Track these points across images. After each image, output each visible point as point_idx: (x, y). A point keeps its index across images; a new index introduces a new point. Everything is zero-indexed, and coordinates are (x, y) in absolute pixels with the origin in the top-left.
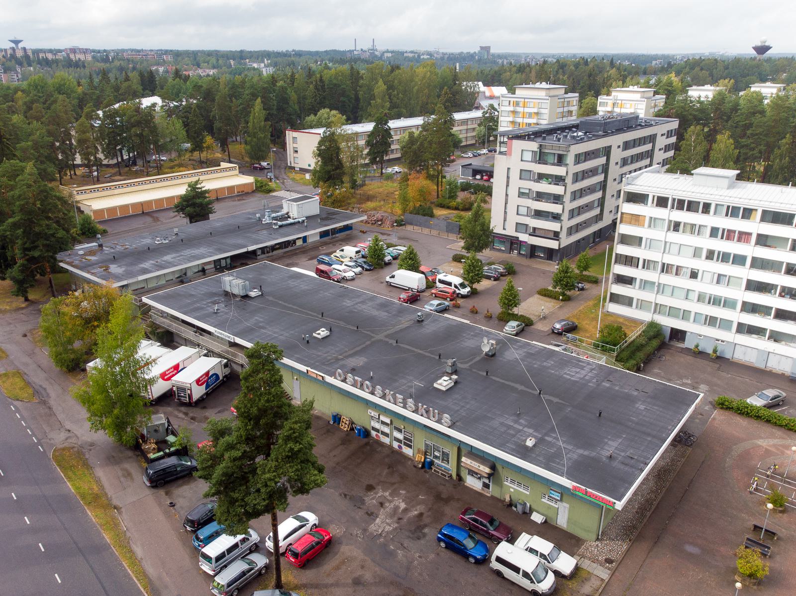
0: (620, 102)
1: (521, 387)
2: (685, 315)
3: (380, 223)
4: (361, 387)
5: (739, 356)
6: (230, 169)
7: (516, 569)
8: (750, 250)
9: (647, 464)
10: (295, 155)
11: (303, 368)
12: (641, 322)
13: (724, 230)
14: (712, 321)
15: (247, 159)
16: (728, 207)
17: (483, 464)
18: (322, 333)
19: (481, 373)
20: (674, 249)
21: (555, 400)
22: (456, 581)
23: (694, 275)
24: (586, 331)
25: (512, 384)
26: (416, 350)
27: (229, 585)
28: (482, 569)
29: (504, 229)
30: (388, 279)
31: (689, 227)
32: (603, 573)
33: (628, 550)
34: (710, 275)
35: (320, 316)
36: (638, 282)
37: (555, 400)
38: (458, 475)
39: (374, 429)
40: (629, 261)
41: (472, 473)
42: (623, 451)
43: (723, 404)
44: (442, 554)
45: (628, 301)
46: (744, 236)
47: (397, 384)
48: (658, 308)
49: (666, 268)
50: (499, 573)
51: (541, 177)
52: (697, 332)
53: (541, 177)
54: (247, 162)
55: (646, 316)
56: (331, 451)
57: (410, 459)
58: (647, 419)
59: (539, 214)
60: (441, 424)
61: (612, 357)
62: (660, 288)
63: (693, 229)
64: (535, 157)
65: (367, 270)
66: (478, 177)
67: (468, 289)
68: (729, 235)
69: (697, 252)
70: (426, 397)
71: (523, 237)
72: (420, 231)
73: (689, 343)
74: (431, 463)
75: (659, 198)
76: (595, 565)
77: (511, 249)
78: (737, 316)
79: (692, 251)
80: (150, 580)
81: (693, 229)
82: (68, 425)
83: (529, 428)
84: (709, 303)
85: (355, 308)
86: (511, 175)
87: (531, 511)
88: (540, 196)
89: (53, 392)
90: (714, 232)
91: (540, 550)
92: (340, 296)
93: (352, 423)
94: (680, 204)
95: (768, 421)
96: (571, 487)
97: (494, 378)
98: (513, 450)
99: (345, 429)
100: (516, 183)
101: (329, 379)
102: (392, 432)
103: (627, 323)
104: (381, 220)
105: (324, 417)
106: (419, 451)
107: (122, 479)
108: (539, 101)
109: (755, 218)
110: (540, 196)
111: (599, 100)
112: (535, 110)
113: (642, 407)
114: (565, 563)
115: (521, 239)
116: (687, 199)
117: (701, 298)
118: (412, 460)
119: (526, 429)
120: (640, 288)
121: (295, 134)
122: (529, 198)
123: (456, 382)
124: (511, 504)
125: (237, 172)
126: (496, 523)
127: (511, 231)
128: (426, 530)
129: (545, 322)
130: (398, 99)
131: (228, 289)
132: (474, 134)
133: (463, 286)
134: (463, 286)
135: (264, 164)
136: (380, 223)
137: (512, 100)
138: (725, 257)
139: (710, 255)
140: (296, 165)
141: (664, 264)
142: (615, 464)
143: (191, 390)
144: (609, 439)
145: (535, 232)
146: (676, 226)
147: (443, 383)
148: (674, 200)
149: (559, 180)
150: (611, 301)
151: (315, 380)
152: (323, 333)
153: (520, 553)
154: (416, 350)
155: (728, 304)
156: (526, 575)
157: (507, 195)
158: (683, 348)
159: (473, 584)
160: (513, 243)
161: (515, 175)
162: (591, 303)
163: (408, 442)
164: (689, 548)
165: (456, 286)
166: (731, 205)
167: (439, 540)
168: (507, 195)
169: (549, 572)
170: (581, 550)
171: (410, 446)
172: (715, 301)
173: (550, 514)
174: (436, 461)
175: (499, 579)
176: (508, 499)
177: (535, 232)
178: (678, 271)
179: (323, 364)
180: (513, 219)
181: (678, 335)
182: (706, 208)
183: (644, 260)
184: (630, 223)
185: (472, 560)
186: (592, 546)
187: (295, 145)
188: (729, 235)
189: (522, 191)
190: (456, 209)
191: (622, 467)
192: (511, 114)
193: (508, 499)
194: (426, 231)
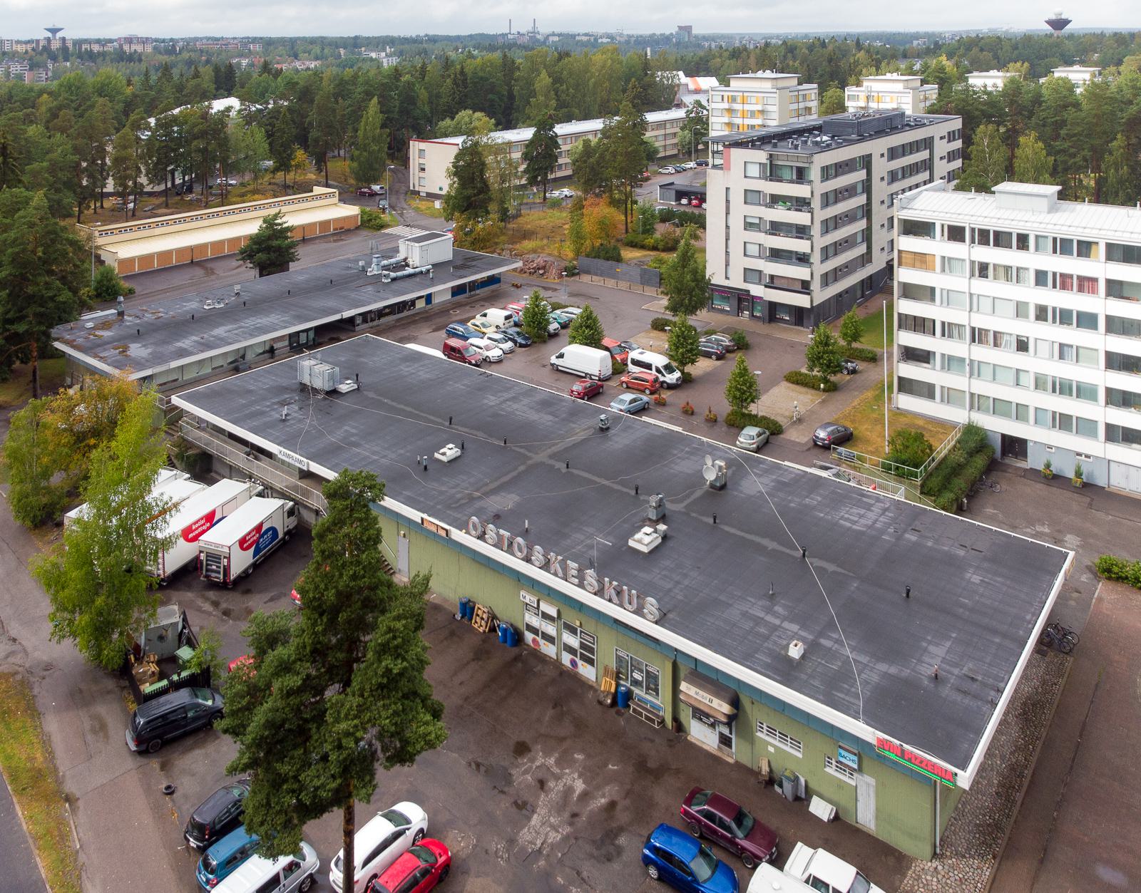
1: (771, 545)
2: (1020, 412)
3: (541, 272)
4: (510, 550)
6: (326, 196)
10: (422, 174)
11: (415, 515)
12: (953, 426)
14: (1063, 422)
17: (717, 695)
21: (831, 567)
24: (867, 441)
29: (727, 278)
30: (553, 360)
35: (447, 423)
36: (938, 357)
42: (956, 665)
43: (1109, 571)
45: (927, 391)
46: (1086, 284)
48: (976, 402)
49: (977, 336)
51: (775, 200)
53: (775, 200)
54: (351, 186)
55: (959, 415)
56: (455, 674)
57: (591, 687)
58: (988, 602)
59: (776, 255)
62: (975, 369)
64: (764, 172)
65: (521, 346)
66: (684, 201)
67: (677, 374)
68: (1064, 281)
70: (616, 566)
71: (757, 290)
73: (1035, 461)
75: (950, 227)
77: (740, 310)
83: (791, 621)
87: (809, 793)
90: (1041, 278)
92: (480, 389)
94: (983, 237)
97: (727, 528)
98: (767, 666)
99: (481, 630)
103: (930, 427)
104: (544, 268)
107: (89, 737)
109: (1097, 256)
111: (847, 93)
112: (759, 107)
113: (976, 579)
115: (752, 293)
119: (786, 625)
120: (943, 368)
122: (760, 231)
123: (665, 538)
124: (771, 781)
125: (336, 200)
126: (748, 823)
127: (737, 282)
130: (567, 95)
133: (669, 369)
134: (669, 369)
135: (376, 188)
136: (541, 272)
137: (726, 94)
138: (1064, 317)
140: (421, 189)
142: (945, 691)
143: (229, 559)
144: (930, 643)
145: (773, 282)
146: (983, 270)
147: (644, 539)
157: (727, 227)
158: (1025, 470)
160: (742, 300)
161: (737, 198)
165: (658, 370)
168: (727, 227)
173: (844, 801)
174: (636, 691)
176: (765, 769)
177: (773, 282)
178: (997, 339)
179: (449, 507)
180: (739, 263)
181: (1015, 446)
182: (1023, 242)
187: (422, 161)
188: (1064, 281)
189: (749, 220)
190: (655, 248)
191: (959, 697)
192: (725, 113)
193: (765, 769)
194: (611, 283)
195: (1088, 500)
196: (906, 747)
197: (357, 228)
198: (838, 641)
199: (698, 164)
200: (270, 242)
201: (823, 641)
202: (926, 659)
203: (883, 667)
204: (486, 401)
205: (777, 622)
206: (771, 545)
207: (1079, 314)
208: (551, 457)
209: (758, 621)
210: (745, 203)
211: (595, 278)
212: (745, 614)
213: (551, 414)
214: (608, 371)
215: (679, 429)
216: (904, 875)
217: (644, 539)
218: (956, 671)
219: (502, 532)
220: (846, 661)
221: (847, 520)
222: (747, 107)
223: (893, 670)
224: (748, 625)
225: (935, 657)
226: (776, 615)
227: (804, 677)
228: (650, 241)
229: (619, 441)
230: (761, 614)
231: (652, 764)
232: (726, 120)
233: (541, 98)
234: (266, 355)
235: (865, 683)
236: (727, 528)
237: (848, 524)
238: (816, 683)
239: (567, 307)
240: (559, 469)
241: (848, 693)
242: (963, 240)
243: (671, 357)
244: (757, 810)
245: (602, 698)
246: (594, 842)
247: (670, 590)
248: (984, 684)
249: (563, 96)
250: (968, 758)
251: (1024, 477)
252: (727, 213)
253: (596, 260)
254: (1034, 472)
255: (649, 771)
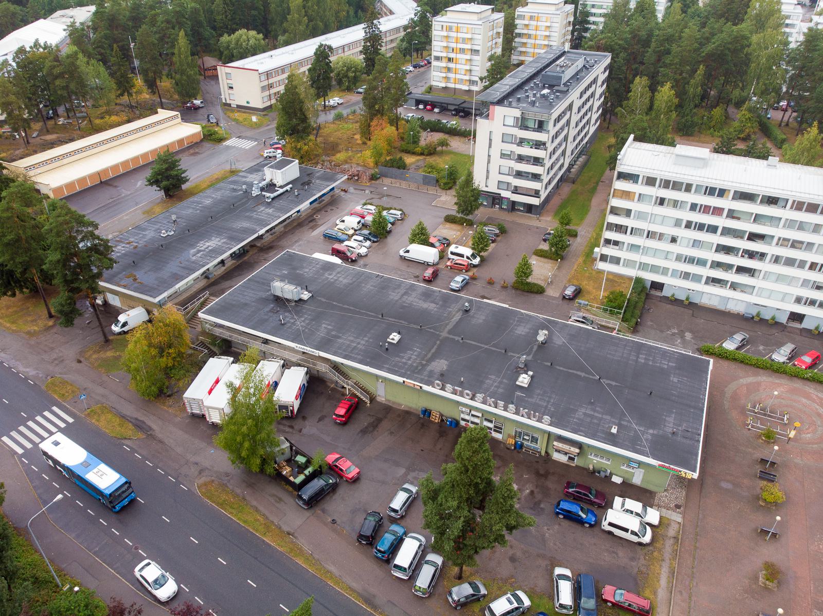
0: (536, 15)
1: (583, 374)
2: (665, 271)
3: (356, 178)
4: (462, 395)
5: (705, 301)
6: (173, 118)
7: (626, 530)
8: (721, 222)
9: (700, 435)
10: (230, 91)
11: (401, 380)
12: (630, 278)
13: (701, 205)
14: (686, 276)
15: (176, 97)
16: (707, 187)
17: (573, 446)
18: (395, 338)
19: (546, 364)
20: (659, 219)
21: (614, 383)
22: (581, 544)
23: (674, 240)
24: (589, 293)
25: (575, 372)
26: (483, 346)
27: (429, 587)
28: (596, 529)
29: (486, 186)
30: (402, 253)
31: (672, 203)
32: (677, 517)
33: (687, 495)
34: (686, 241)
35: (380, 316)
36: (626, 245)
37: (614, 383)
38: (546, 452)
39: (463, 419)
40: (620, 228)
41: (558, 451)
42: (680, 425)
43: (708, 351)
44: (562, 524)
45: (616, 261)
46: (718, 211)
47: (485, 386)
48: (643, 266)
49: (650, 235)
50: (610, 533)
51: (521, 142)
52: (674, 285)
53: (521, 142)
54: (177, 100)
55: (632, 273)
56: (435, 445)
57: (501, 442)
58: (684, 391)
59: (519, 174)
60: (542, 422)
61: (619, 318)
62: (646, 251)
63: (675, 204)
64: (517, 123)
65: (374, 242)
66: (421, 107)
67: (478, 259)
68: (706, 209)
69: (678, 223)
70: (510, 395)
71: (505, 194)
72: (398, 185)
73: (666, 292)
74: (522, 446)
75: (648, 178)
76: (670, 512)
77: (493, 204)
78: (707, 272)
79: (673, 222)
80: (358, 593)
81: (675, 204)
82: (193, 459)
83: (606, 414)
84: (685, 262)
85: (404, 302)
86: (493, 138)
87: (611, 474)
88: (521, 158)
89: (154, 424)
90: (693, 207)
91: (634, 510)
92: (383, 288)
93: (441, 415)
94: (666, 184)
95: (742, 362)
96: (657, 465)
97: (558, 367)
98: (605, 439)
99: (436, 421)
100: (499, 146)
101: (426, 388)
102: (482, 422)
103: (616, 279)
104: (358, 175)
105: (412, 410)
106: (509, 436)
107: (277, 505)
108: (472, 26)
109: (727, 197)
110: (521, 158)
111: (517, 13)
112: (469, 36)
113: (675, 380)
114: (653, 516)
115: (502, 195)
116: (672, 179)
117: (679, 258)
118: (504, 443)
119: (604, 417)
120: (627, 250)
121: (228, 70)
122: (511, 159)
123: (532, 377)
124: (594, 472)
125: (179, 120)
126: (594, 492)
127: (493, 188)
128: (542, 506)
129: (553, 287)
130: (313, 11)
131: (279, 294)
132: (394, 45)
133: (474, 256)
134: (474, 256)
135: (197, 102)
136: (356, 178)
137: (445, 24)
138: (701, 227)
139: (689, 225)
140: (231, 102)
141: (649, 232)
142: (679, 439)
143: (293, 407)
144: (666, 416)
145: (516, 190)
146: (662, 202)
147: (524, 380)
148: (661, 180)
149: (539, 145)
150: (601, 260)
151: (413, 388)
152: (395, 337)
153: (622, 515)
154: (483, 346)
155: (701, 262)
156: (633, 533)
157: (489, 156)
158: (661, 297)
159: (595, 544)
160: (495, 199)
161: (497, 139)
162: (581, 260)
163: (498, 429)
164: (724, 485)
165: (468, 258)
166: (710, 185)
167: (558, 513)
168: (489, 156)
169: (648, 528)
170: (656, 501)
171: (500, 433)
172: (691, 260)
173: (627, 476)
174: (525, 443)
175: (610, 536)
176: (591, 467)
177: (516, 190)
178: (661, 237)
179: (413, 372)
180: (495, 177)
181: (658, 286)
182: (688, 188)
183: (632, 228)
184: (621, 198)
185: (587, 525)
186: (662, 497)
187: (229, 81)
188: (706, 209)
189: (503, 152)
190: (422, 154)
191: (685, 441)
192: (444, 39)
193: (591, 467)
194: (404, 185)
195: (691, 312)
196: (671, 466)
197: (202, 141)
198: (629, 421)
199: (415, 67)
200: (169, 173)
201: (622, 422)
202: (667, 424)
203: (651, 431)
204: (392, 297)
205: (600, 416)
206: (583, 374)
207: (709, 226)
208: (450, 332)
209: (592, 417)
210: (502, 141)
211: (393, 180)
212: (585, 414)
213: (432, 302)
214: (437, 259)
215: (507, 306)
216: (654, 499)
217: (524, 380)
218: (680, 428)
219: (456, 388)
220: (635, 431)
221: (610, 354)
222: (460, 35)
223: (655, 432)
224: (588, 420)
225: (670, 424)
226: (598, 412)
227: (621, 441)
228: (418, 150)
229: (479, 318)
230: (592, 413)
231: (542, 472)
232: (445, 44)
233: (296, 16)
234: (221, 265)
235: (647, 440)
236: (558, 367)
237: (611, 357)
238: (627, 443)
239: (391, 209)
240: (458, 341)
241: (640, 445)
242: (654, 185)
243: (473, 249)
244: (596, 486)
245: (508, 446)
246: (531, 508)
247: (546, 407)
248: (692, 433)
249: (310, 12)
250: (696, 467)
251: (660, 301)
252: (490, 146)
253: (391, 169)
254: (666, 298)
255: (542, 475)
